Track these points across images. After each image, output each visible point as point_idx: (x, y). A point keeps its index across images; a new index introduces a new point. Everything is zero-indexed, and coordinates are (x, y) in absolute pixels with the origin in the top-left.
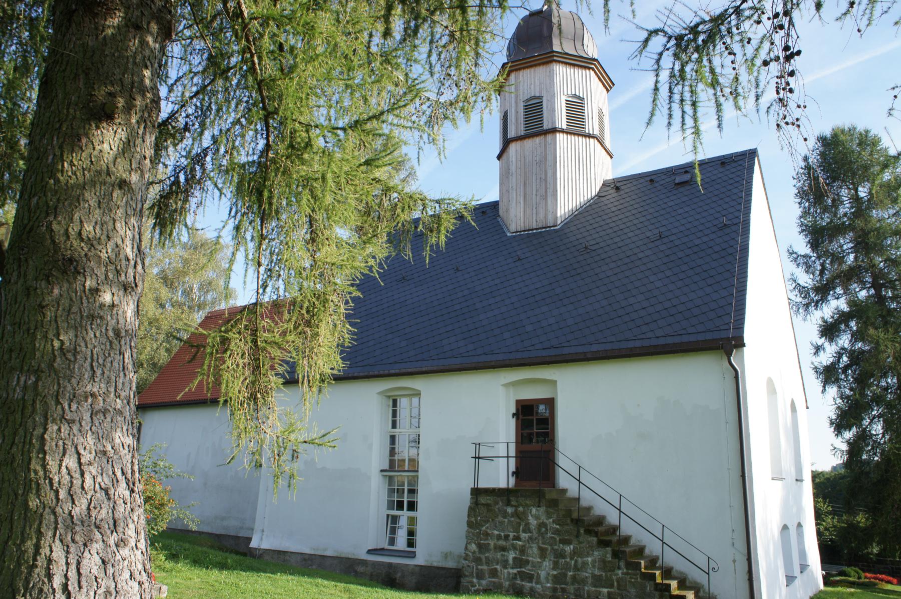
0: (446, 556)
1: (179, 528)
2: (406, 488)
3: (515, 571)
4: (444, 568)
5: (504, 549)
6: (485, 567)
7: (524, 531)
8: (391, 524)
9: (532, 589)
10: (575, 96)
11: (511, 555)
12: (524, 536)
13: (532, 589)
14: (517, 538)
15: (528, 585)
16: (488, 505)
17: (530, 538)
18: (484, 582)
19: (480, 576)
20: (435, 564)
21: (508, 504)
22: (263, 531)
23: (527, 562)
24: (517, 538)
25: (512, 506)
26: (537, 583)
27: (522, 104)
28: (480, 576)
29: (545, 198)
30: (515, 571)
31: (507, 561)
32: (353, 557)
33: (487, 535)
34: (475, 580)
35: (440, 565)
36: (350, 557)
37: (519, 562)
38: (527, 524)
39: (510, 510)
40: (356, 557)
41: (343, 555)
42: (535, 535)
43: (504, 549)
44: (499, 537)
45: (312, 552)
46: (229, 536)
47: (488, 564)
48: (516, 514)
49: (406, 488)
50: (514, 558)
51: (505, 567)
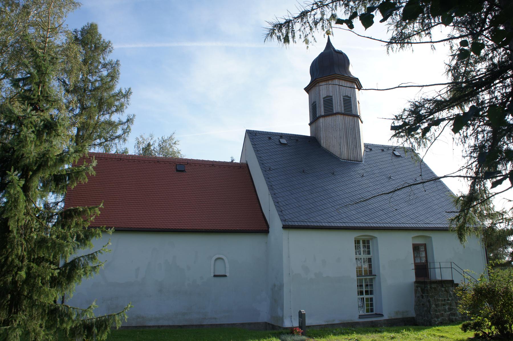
0: (397, 313)
1: (134, 325)
2: (364, 284)
3: (449, 313)
4: (396, 319)
5: (444, 305)
6: (438, 313)
7: (450, 297)
8: (366, 302)
9: (455, 319)
10: (347, 96)
11: (447, 307)
12: (450, 298)
13: (455, 319)
14: (448, 300)
15: (454, 317)
16: (435, 288)
17: (452, 299)
18: (439, 319)
19: (438, 317)
20: (393, 318)
21: (442, 287)
22: (291, 316)
23: (453, 309)
24: (448, 300)
25: (444, 287)
26: (457, 316)
27: (342, 97)
28: (438, 317)
29: (356, 147)
30: (449, 313)
31: (446, 309)
32: (351, 322)
33: (438, 300)
34: (436, 319)
35: (395, 317)
36: (349, 322)
37: (450, 309)
38: (450, 294)
39: (443, 289)
40: (353, 321)
41: (346, 322)
42: (453, 298)
43: (444, 305)
44: (442, 300)
45: (326, 323)
46: (193, 325)
47: (439, 312)
48: (446, 291)
49: (364, 284)
50: (448, 308)
51: (445, 312)
